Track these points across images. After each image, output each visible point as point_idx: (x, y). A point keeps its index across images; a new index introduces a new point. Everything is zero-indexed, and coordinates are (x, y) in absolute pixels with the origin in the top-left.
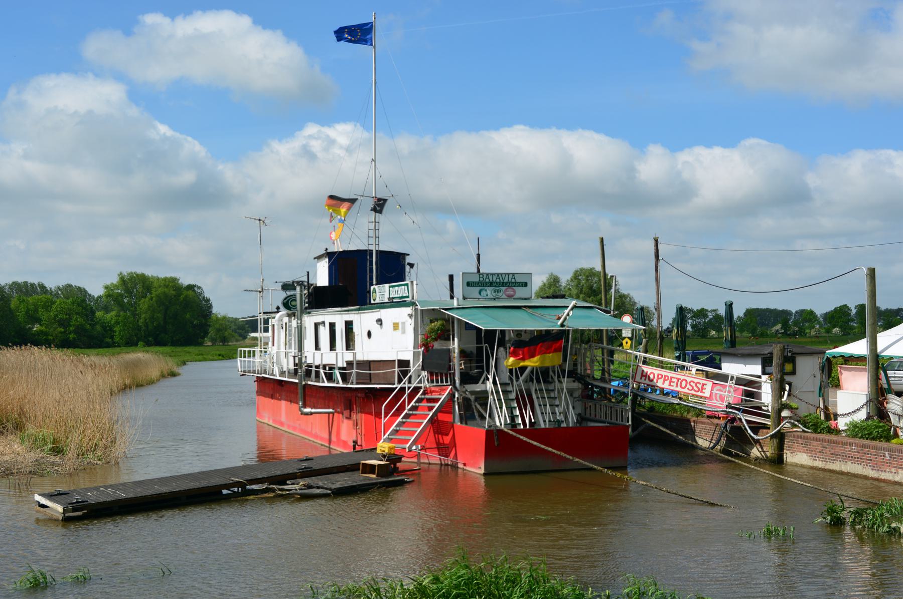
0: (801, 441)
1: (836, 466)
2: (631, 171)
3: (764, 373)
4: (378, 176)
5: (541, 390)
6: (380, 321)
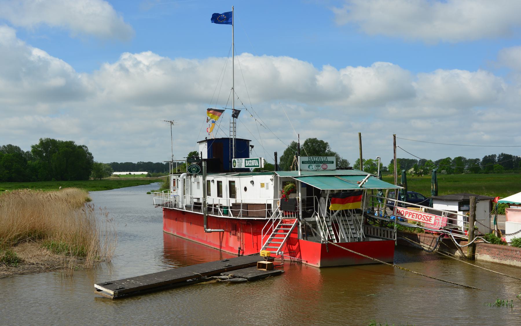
0: (485, 248)
1: (508, 262)
2: (313, 80)
3: (460, 210)
4: (236, 98)
5: (345, 221)
6: (252, 182)
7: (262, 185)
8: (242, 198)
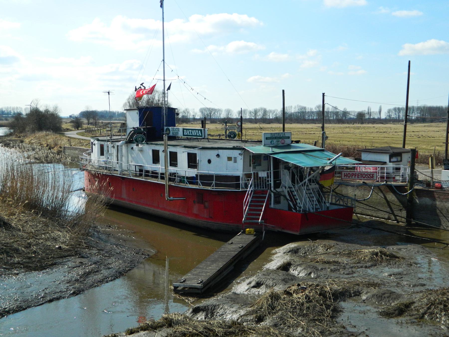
3: (390, 162)
7: (229, 159)
8: (204, 169)
